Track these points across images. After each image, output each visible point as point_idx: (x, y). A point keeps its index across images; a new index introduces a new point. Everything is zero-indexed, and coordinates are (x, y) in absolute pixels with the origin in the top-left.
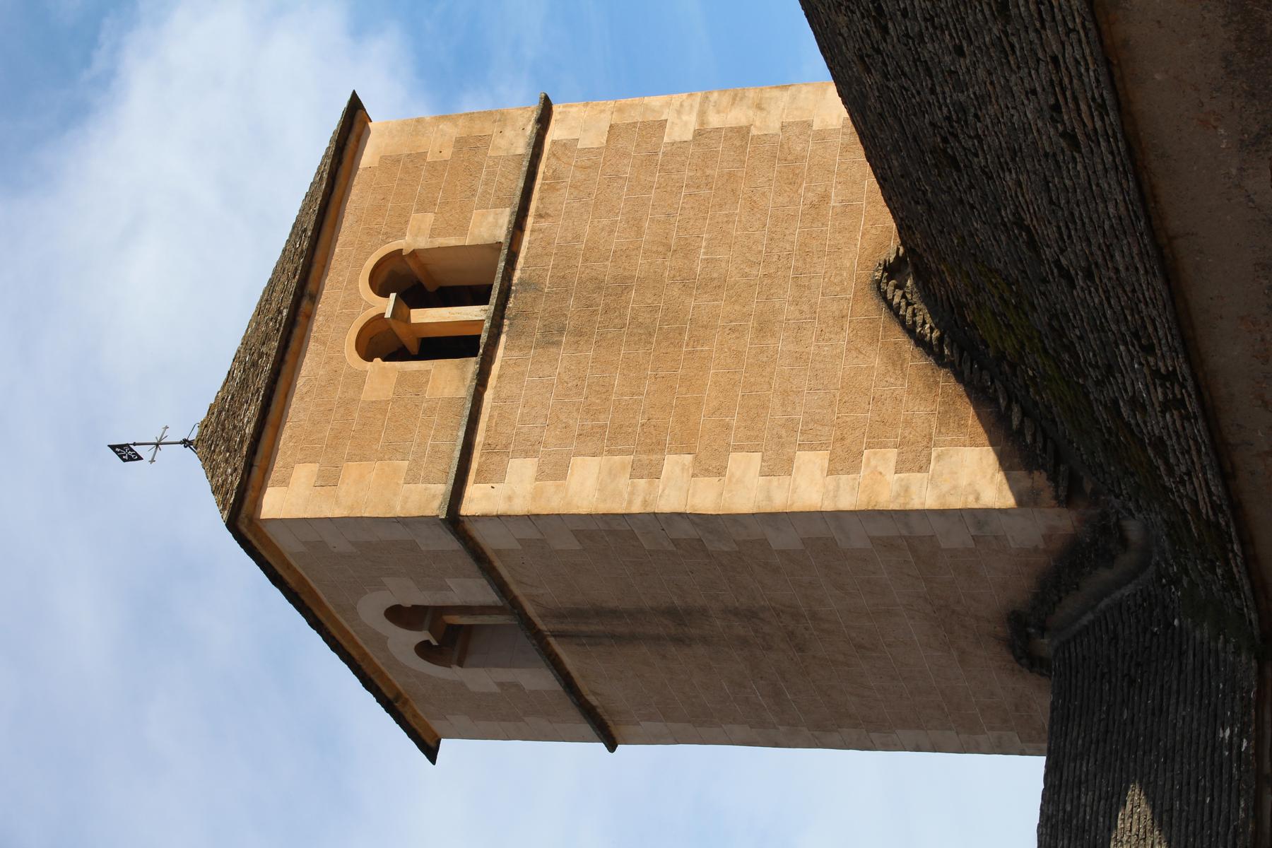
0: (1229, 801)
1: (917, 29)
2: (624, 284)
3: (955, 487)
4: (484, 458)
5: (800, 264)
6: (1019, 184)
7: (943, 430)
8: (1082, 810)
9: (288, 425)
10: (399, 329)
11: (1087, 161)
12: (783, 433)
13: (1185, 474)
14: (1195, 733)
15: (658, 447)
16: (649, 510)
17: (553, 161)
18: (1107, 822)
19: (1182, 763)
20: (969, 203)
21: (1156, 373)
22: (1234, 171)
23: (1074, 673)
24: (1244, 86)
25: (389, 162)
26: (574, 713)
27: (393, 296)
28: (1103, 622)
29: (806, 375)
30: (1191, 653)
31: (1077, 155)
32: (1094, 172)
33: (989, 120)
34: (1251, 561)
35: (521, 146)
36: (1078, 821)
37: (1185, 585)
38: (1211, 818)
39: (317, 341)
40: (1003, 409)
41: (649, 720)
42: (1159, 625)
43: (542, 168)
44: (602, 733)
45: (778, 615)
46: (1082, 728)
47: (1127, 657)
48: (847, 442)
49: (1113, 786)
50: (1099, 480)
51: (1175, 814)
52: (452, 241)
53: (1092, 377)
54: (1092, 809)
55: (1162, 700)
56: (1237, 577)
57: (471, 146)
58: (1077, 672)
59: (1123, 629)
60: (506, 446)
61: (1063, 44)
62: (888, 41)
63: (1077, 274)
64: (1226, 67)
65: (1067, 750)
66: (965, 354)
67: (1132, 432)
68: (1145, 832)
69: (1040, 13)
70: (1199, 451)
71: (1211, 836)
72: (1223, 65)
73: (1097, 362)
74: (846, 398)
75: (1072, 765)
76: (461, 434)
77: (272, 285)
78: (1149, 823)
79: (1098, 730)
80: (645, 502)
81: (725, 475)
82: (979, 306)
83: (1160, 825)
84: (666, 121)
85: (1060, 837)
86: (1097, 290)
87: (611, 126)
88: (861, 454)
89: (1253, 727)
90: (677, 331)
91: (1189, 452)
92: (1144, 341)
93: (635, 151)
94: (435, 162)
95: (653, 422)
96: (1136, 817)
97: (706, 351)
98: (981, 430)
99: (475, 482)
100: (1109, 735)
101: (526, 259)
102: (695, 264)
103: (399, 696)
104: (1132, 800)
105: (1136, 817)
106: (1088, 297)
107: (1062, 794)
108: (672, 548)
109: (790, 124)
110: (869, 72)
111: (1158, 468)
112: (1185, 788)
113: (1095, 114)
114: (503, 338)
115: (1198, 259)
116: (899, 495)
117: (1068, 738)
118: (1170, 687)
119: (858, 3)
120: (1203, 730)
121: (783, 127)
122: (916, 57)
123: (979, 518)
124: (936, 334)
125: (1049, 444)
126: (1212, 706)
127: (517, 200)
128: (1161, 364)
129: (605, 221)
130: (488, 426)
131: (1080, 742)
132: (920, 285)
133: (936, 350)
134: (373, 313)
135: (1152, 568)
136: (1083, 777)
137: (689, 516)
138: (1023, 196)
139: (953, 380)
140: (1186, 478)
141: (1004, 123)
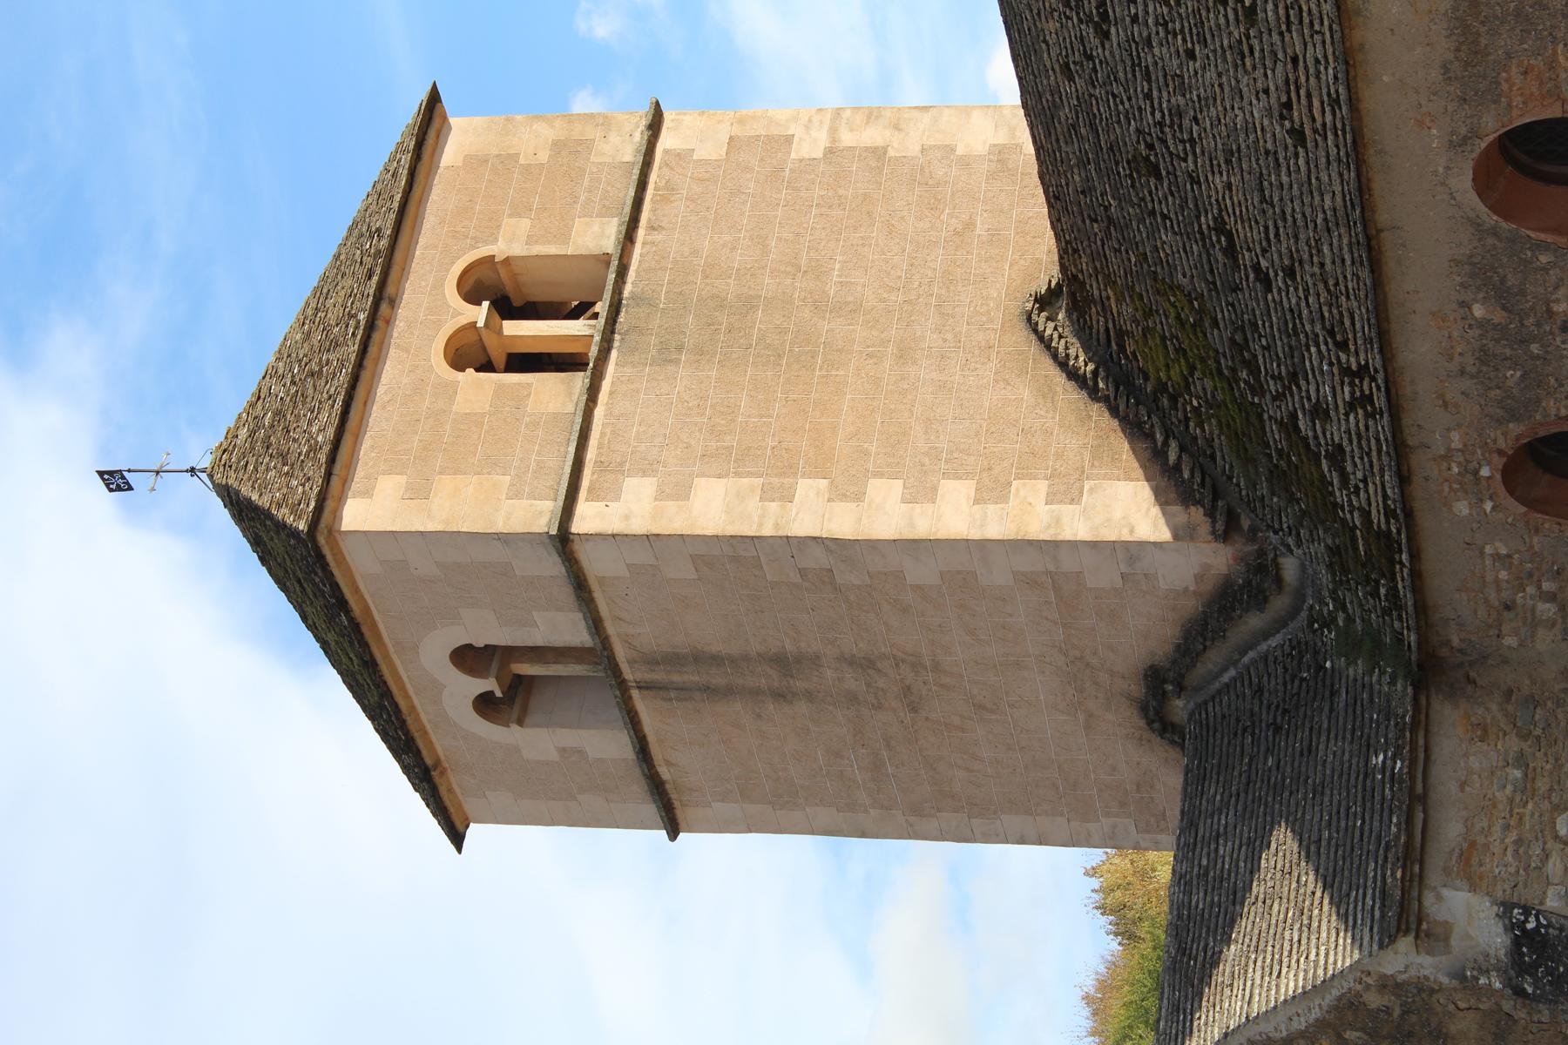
0: (1381, 821)
1: (1145, 34)
2: (748, 304)
3: (1109, 520)
4: (595, 476)
5: (943, 292)
6: (1229, 186)
7: (1096, 463)
8: (1220, 861)
9: (368, 434)
10: (491, 342)
11: (1310, 155)
12: (926, 461)
13: (1360, 481)
14: (1346, 765)
15: (790, 470)
16: (781, 533)
17: (666, 170)
18: (1249, 865)
19: (1332, 795)
20: (1162, 213)
21: (1346, 371)
22: (1441, 170)
23: (1211, 733)
24: (1458, 91)
25: (475, 162)
26: (638, 787)
27: (486, 304)
28: (1246, 678)
29: (950, 404)
30: (1344, 690)
31: (1300, 150)
32: (1316, 166)
33: (1208, 122)
34: (1416, 575)
35: (625, 146)
36: (1215, 873)
37: (1341, 624)
38: (1362, 840)
39: (398, 346)
40: (1159, 444)
41: (723, 801)
42: (1309, 671)
43: (653, 177)
44: (667, 815)
45: (897, 665)
46: (1220, 784)
47: (1273, 707)
48: (995, 472)
49: (1256, 831)
50: (1257, 516)
51: (1324, 843)
52: (553, 250)
53: (1271, 392)
54: (1231, 858)
55: (1311, 741)
56: (1401, 593)
57: (570, 151)
58: (1215, 731)
59: (1269, 681)
60: (622, 464)
61: (1305, 45)
62: (1107, 46)
63: (1276, 275)
64: (1445, 74)
65: (1203, 808)
66: (1121, 388)
67: (1307, 446)
68: (1291, 866)
69: (1288, 16)
70: (1379, 451)
71: (1361, 856)
72: (1442, 71)
73: (1280, 373)
74: (993, 429)
75: (1209, 821)
76: (572, 449)
77: (321, 293)
78: (1296, 856)
79: (1239, 783)
80: (777, 525)
81: (863, 501)
82: (1146, 331)
83: (1308, 856)
84: (793, 136)
85: (1194, 891)
86: (1296, 289)
87: (731, 138)
88: (1010, 484)
89: (1408, 748)
90: (810, 354)
91: (1369, 454)
92: (1339, 337)
93: (759, 166)
94: (530, 165)
95: (784, 445)
96: (1281, 854)
97: (842, 375)
98: (1136, 465)
99: (587, 500)
100: (1251, 785)
101: (637, 272)
102: (829, 286)
103: (438, 763)
104: (1277, 839)
105: (1281, 854)
106: (1285, 299)
107: (1198, 850)
108: (797, 579)
109: (931, 147)
110: (1071, 79)
111: (1332, 484)
112: (1335, 818)
113: (1327, 109)
114: (614, 354)
115: (1400, 252)
116: (1049, 526)
117: (1205, 797)
118: (1320, 727)
119: (1077, 6)
120: (1354, 761)
121: (923, 150)
122: (1136, 62)
123: (1131, 551)
124: (1091, 367)
125: (1207, 479)
126: (1365, 736)
127: (628, 209)
128: (1353, 360)
129: (727, 237)
130: (600, 443)
131: (1218, 798)
132: (1074, 317)
133: (1090, 383)
134: (463, 321)
135: (1304, 614)
136: (1222, 829)
137: (825, 541)
138: (1231, 198)
139: (1107, 414)
140: (1361, 485)
141: (1226, 125)
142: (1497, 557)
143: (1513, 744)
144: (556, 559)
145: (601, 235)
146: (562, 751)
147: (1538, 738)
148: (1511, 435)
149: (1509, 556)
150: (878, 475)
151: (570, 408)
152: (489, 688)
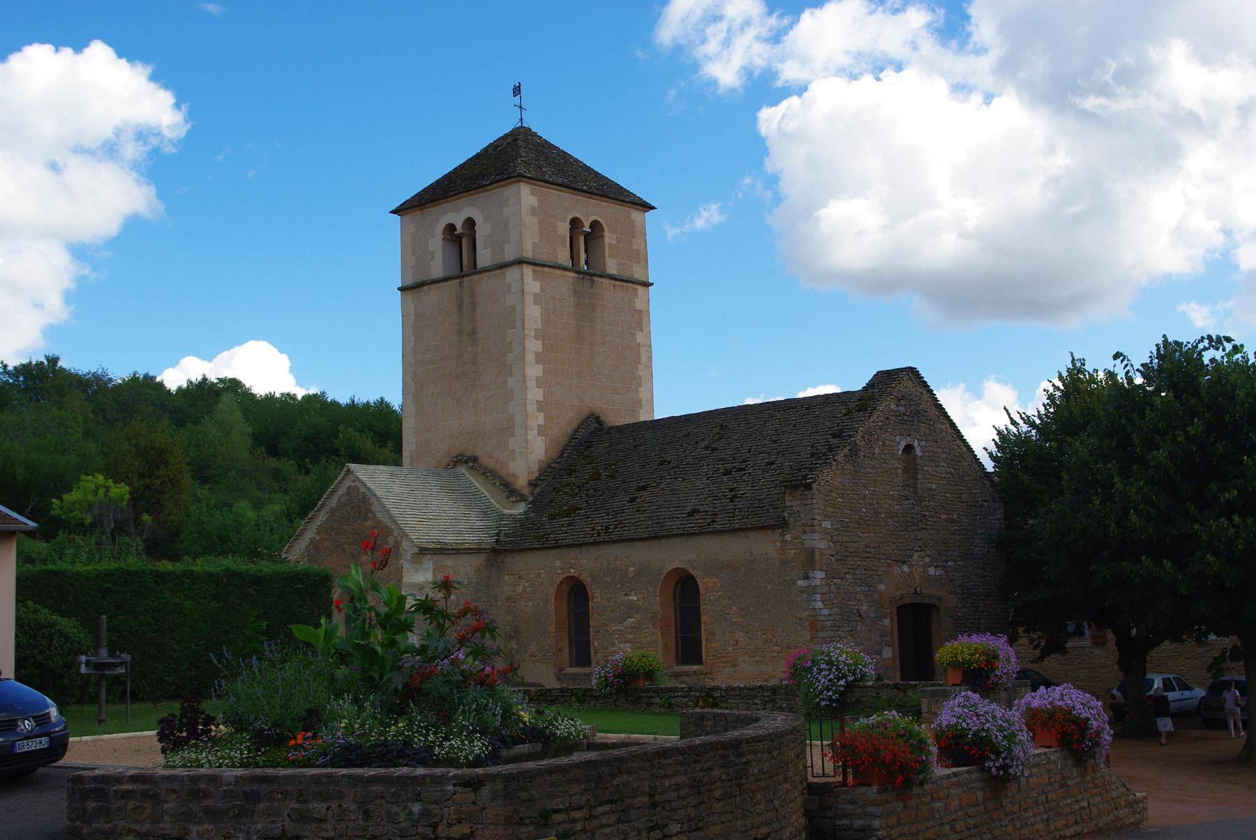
26: (420, 278)
52: (607, 252)
87: (641, 311)
108: (508, 341)
142: (540, 574)
143: (474, 580)
144: (512, 259)
145: (612, 267)
146: (433, 252)
147: (476, 588)
148: (586, 578)
149: (540, 577)
150: (543, 367)
151: (560, 262)
152: (458, 230)
